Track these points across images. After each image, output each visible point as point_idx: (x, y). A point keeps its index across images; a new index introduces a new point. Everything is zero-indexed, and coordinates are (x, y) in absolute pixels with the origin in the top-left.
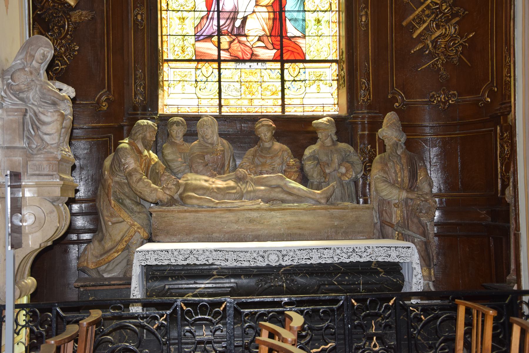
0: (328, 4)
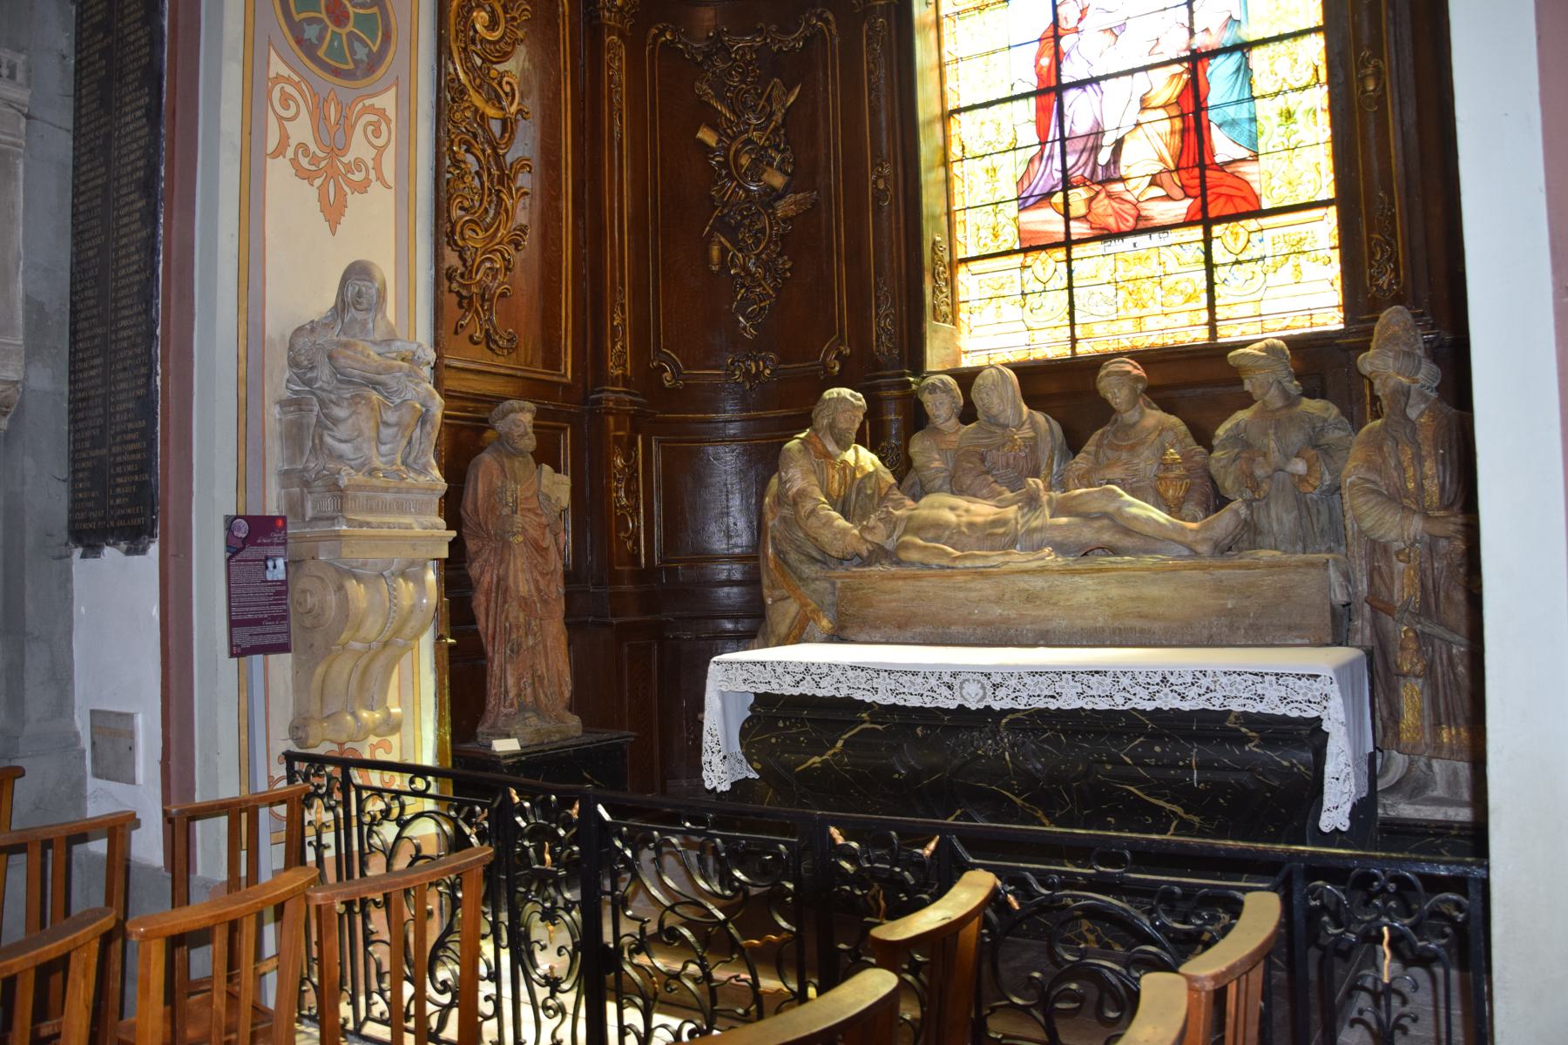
0: (1311, 71)
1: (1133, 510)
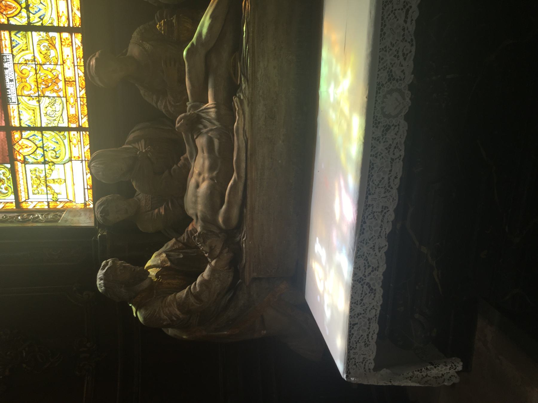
1: (205, 31)
